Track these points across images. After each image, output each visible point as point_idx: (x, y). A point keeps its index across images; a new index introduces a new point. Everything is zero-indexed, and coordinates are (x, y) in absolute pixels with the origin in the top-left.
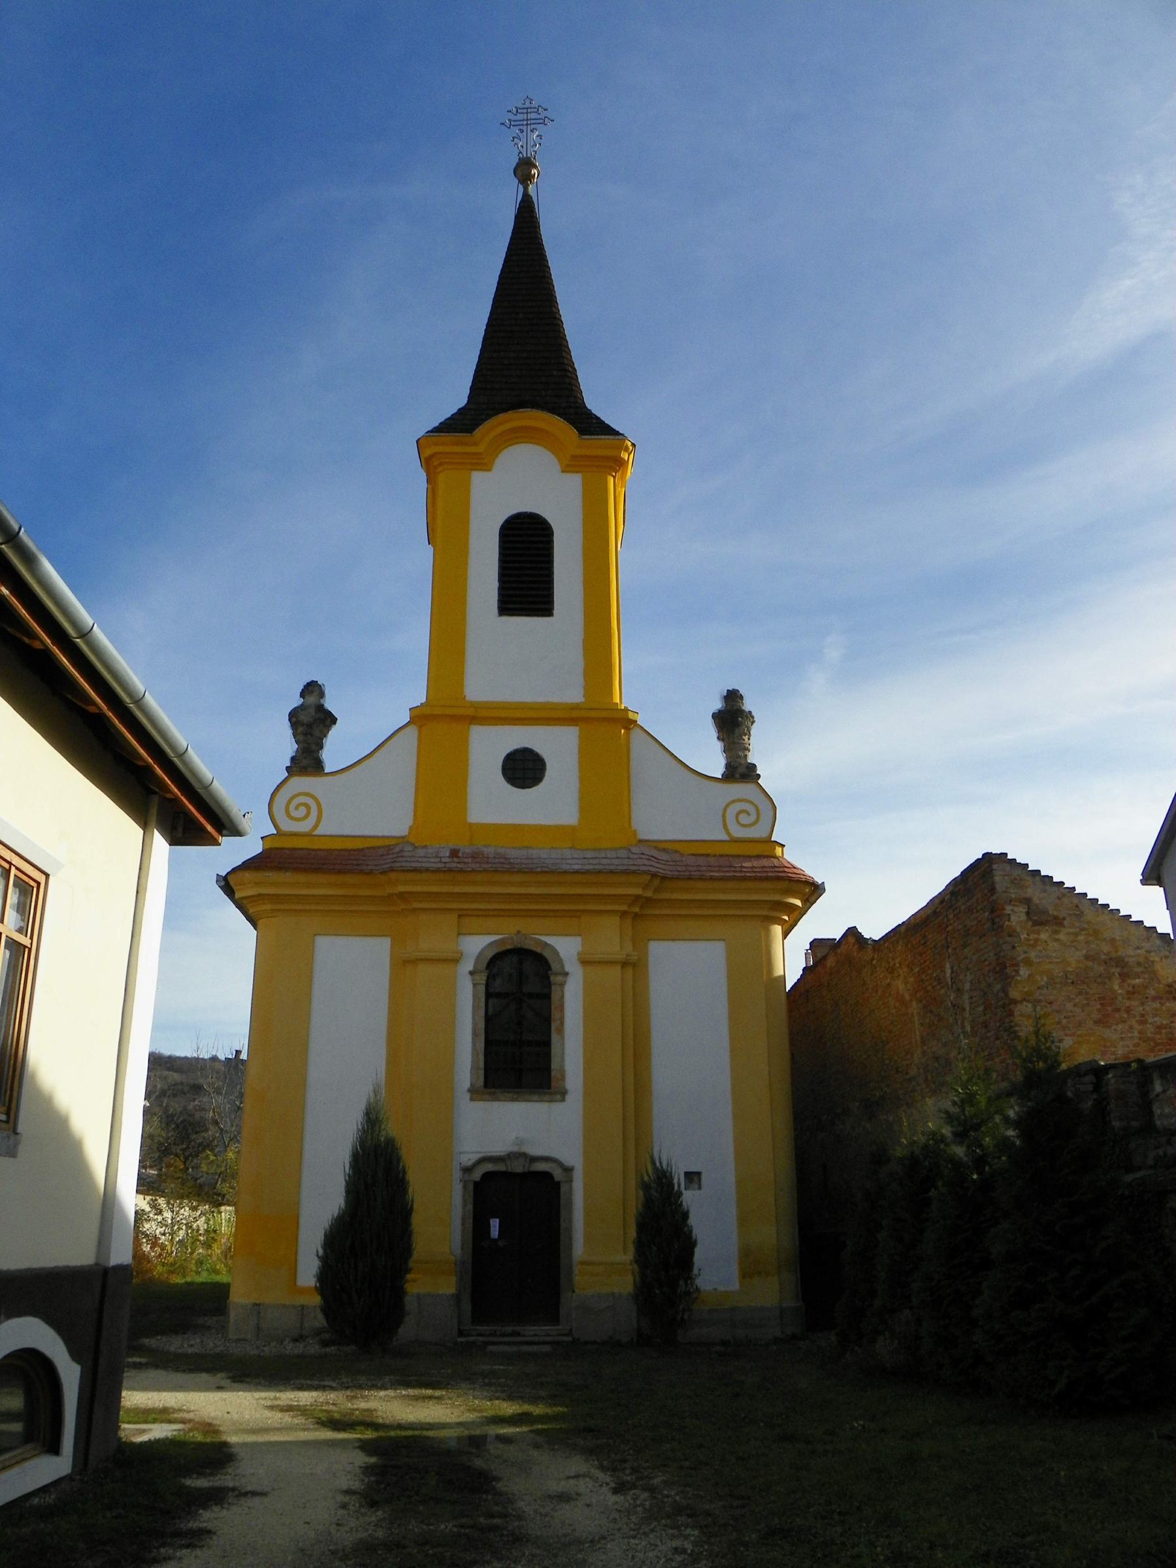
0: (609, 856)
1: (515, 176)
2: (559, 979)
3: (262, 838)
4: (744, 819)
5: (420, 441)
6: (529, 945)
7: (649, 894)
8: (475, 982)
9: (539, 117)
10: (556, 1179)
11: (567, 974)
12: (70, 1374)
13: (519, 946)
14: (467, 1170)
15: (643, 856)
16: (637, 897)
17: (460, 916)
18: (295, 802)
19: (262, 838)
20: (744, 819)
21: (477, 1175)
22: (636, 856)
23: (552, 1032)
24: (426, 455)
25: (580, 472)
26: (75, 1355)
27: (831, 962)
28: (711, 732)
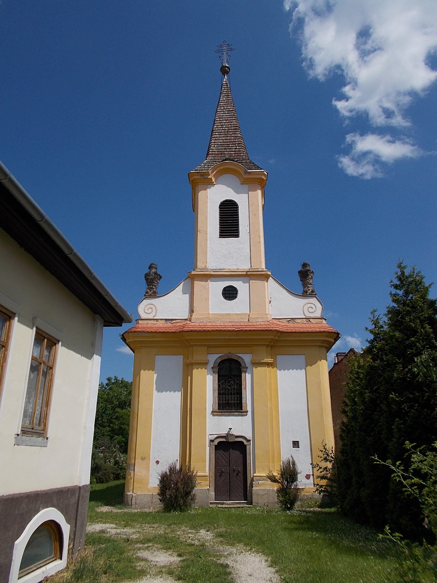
0: (233, 135)
1: (221, 71)
2: (244, 369)
3: (136, 320)
4: (311, 310)
5: (190, 174)
6: (234, 357)
7: (277, 338)
8: (214, 371)
9: (229, 48)
10: (245, 444)
11: (247, 368)
12: (66, 529)
13: (230, 358)
14: (212, 441)
15: (274, 324)
16: (272, 339)
17: (208, 347)
18: (146, 309)
19: (136, 320)
20: (311, 310)
21: (216, 442)
22: (272, 324)
23: (242, 389)
24: (191, 180)
25: (248, 184)
26: (68, 521)
27: (345, 361)
28: (298, 278)
